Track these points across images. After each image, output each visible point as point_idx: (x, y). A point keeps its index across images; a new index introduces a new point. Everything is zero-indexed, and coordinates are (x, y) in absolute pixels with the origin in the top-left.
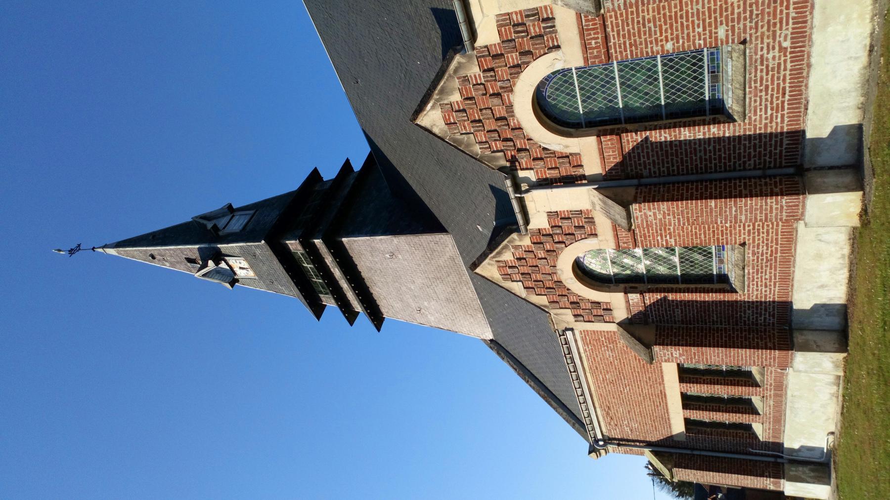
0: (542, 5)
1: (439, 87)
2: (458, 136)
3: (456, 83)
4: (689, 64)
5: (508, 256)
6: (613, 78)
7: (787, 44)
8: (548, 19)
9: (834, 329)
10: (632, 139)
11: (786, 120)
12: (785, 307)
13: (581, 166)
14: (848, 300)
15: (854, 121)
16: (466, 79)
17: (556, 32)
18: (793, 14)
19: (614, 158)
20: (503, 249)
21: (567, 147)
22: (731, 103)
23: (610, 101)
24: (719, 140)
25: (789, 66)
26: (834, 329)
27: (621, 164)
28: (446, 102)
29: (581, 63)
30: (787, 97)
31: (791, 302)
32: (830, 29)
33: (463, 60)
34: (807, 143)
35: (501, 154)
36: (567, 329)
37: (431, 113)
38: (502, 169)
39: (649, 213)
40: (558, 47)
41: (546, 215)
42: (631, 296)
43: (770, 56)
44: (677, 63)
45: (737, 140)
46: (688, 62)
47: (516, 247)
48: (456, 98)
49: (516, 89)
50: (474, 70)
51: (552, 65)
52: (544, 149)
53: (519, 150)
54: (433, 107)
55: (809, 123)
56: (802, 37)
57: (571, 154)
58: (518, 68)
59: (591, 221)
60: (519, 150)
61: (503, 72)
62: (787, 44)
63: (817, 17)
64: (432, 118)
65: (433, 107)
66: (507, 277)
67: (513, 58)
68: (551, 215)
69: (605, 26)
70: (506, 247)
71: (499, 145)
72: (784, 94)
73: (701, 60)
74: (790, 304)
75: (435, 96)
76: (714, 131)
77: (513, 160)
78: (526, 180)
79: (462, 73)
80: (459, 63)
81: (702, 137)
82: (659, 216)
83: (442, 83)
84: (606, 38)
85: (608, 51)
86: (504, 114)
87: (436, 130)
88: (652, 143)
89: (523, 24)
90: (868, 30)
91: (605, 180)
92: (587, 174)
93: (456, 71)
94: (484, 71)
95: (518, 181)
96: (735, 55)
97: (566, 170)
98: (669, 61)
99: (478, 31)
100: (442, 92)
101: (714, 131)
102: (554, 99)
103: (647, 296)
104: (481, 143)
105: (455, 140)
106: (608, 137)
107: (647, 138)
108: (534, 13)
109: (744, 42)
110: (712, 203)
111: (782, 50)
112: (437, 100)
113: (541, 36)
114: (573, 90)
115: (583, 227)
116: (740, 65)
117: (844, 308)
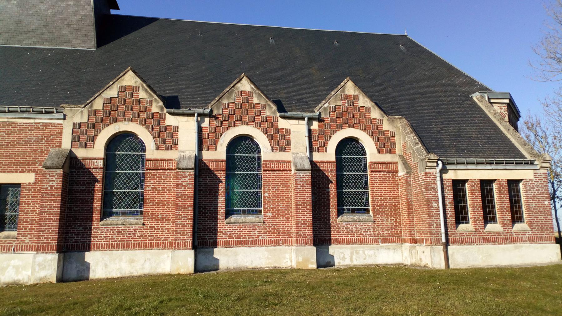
0: (291, 148)
1: (262, 94)
2: (234, 95)
3: (263, 103)
4: (136, 203)
5: (142, 95)
6: (250, 171)
7: (260, 238)
8: (285, 149)
9: (324, 262)
10: (222, 175)
11: (224, 240)
12: (215, 245)
13: (208, 150)
14: (92, 280)
15: (221, 267)
16: (264, 107)
17: (280, 151)
18: (272, 239)
19: (211, 166)
20: (150, 94)
21: (221, 145)
22: (234, 218)
23: (239, 168)
24: (216, 213)
25: (251, 239)
26: (324, 262)
27: (209, 169)
28: (254, 95)
29: (147, 157)
30: (235, 240)
31: (89, 251)
32: (266, 253)
33: (273, 110)
34: (211, 249)
35: (221, 112)
36: (65, 116)
37: (249, 87)
38: (212, 111)
39: (187, 179)
40: (273, 151)
41: (177, 125)
42: (102, 161)
43: (256, 232)
44: (254, 197)
45: (216, 220)
46: (254, 202)
47: (150, 102)
48: (255, 100)
49: (256, 128)
50: (267, 113)
51: (265, 147)
52: (221, 135)
53: (222, 122)
54: (252, 88)
55: (222, 249)
56: (262, 243)
57: (216, 146)
58: (266, 132)
59: (169, 148)
60: (222, 122)
61: (265, 125)
62: (260, 238)
63: (271, 248)
64: (245, 85)
65: (252, 88)
66: (123, 89)
67: (271, 131)
68: (176, 129)
69: (279, 171)
70: (151, 96)
71: (227, 112)
72: (237, 238)
73: (254, 206)
74: (89, 249)
75: (257, 91)
76: (221, 211)
77: (216, 118)
78: (203, 121)
79: (267, 107)
80: (272, 108)
81: (219, 205)
82: (184, 184)
83: (264, 97)
84: (274, 171)
85: (268, 171)
86: (243, 120)
87: (239, 85)
88: (218, 184)
89: (285, 139)
90: (263, 266)
91: (199, 160)
92: (203, 152)
93: (269, 105)
94: (266, 117)
95: (202, 117)
96: (258, 219)
97: (316, 146)
98: (142, 195)
99: (285, 120)
100: (259, 95)
101: (221, 211)
102: (244, 144)
103: (334, 174)
104: (228, 104)
105: (232, 93)
106: (225, 165)
107: (221, 182)
108: (288, 144)
109: (264, 223)
110: (191, 208)
111: (258, 236)
112: (255, 91)
113: (278, 145)
114: (247, 153)
115: (165, 143)
116: (254, 221)
117: (87, 279)
